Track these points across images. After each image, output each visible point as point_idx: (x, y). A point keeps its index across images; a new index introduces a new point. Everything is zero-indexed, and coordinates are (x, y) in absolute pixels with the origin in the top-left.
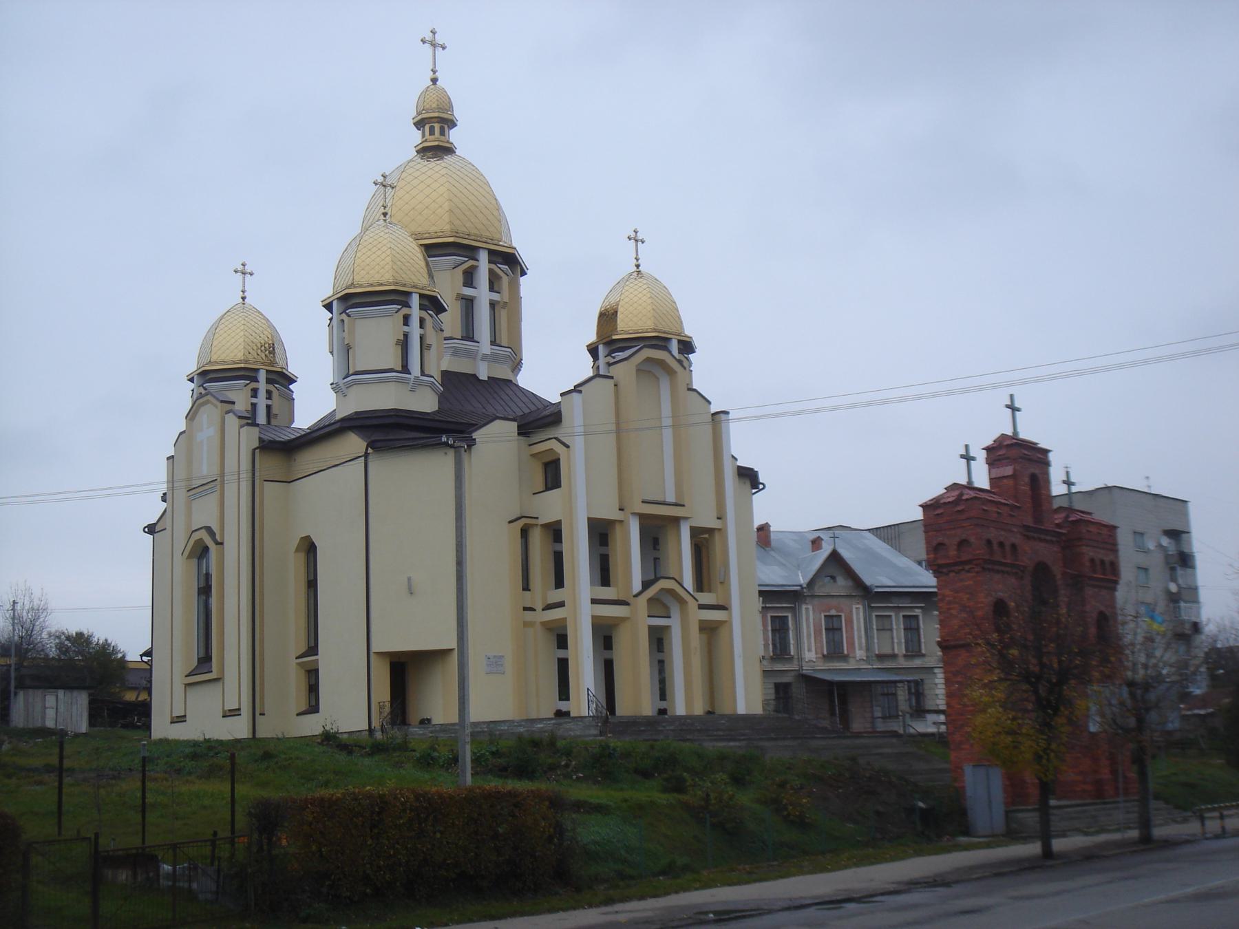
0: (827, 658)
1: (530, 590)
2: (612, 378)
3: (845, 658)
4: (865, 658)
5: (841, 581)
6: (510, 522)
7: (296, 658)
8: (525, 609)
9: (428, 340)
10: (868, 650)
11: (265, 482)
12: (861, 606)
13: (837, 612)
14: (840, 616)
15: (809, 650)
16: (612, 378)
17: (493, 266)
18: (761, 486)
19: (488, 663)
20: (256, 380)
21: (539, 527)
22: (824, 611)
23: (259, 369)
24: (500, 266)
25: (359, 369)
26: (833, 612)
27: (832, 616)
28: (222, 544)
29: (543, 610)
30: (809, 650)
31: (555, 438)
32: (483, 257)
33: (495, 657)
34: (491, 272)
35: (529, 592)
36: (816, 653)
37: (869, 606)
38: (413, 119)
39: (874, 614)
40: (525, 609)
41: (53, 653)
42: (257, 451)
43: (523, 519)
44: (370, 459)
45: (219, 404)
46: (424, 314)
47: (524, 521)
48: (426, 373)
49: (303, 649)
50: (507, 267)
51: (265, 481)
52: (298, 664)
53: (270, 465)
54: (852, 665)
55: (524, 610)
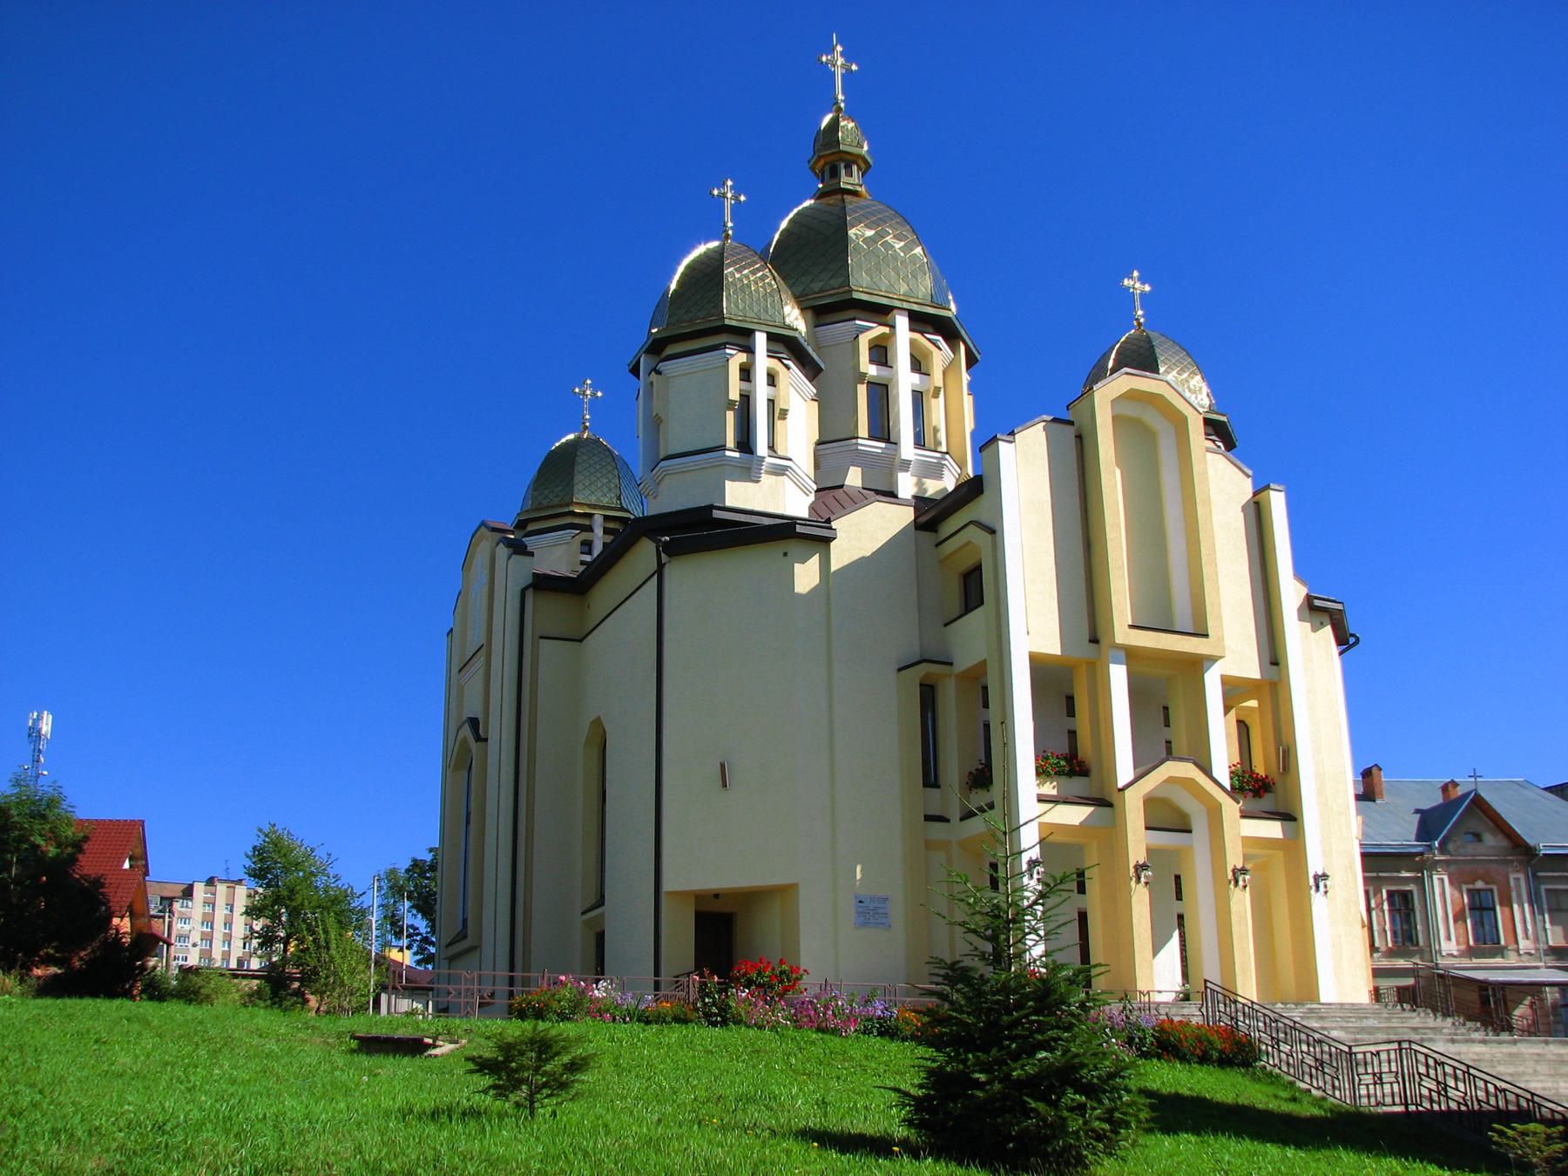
0: (1470, 952)
1: (939, 787)
2: (1071, 423)
3: (1500, 951)
4: (1533, 952)
5: (1491, 840)
6: (899, 670)
7: (583, 913)
8: (928, 818)
9: (782, 401)
10: (1537, 940)
11: (541, 640)
12: (1521, 876)
13: (1487, 883)
14: (1491, 891)
15: (1449, 938)
16: (1071, 423)
17: (917, 336)
18: (1352, 640)
19: (861, 910)
20: (590, 529)
21: (953, 678)
22: (1466, 883)
23: (593, 514)
24: (926, 335)
25: (671, 452)
26: (1480, 885)
27: (1479, 891)
28: (486, 740)
29: (961, 820)
30: (1449, 938)
31: (971, 522)
32: (902, 322)
33: (871, 899)
34: (913, 343)
35: (937, 790)
36: (1458, 943)
37: (1534, 875)
38: (809, 162)
39: (1543, 887)
40: (928, 818)
41: (1025, 1079)
42: (530, 595)
43: (924, 664)
44: (667, 570)
45: (490, 534)
46: (774, 364)
47: (924, 668)
48: (780, 453)
49: (592, 901)
50: (939, 338)
51: (541, 637)
52: (584, 922)
53: (550, 612)
54: (1512, 959)
55: (925, 820)
